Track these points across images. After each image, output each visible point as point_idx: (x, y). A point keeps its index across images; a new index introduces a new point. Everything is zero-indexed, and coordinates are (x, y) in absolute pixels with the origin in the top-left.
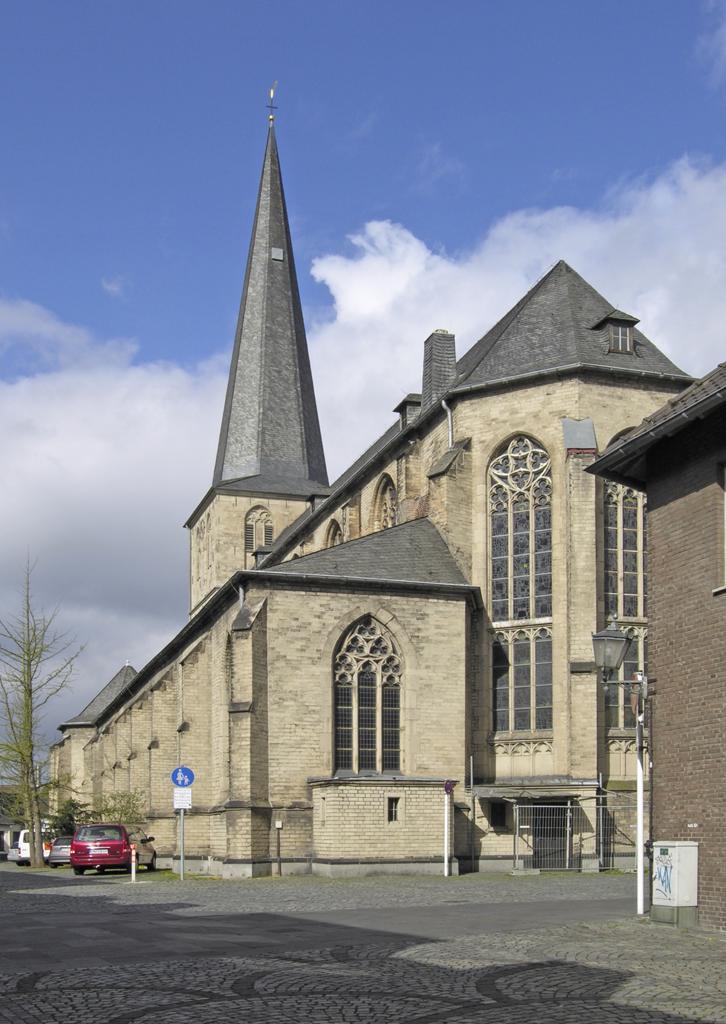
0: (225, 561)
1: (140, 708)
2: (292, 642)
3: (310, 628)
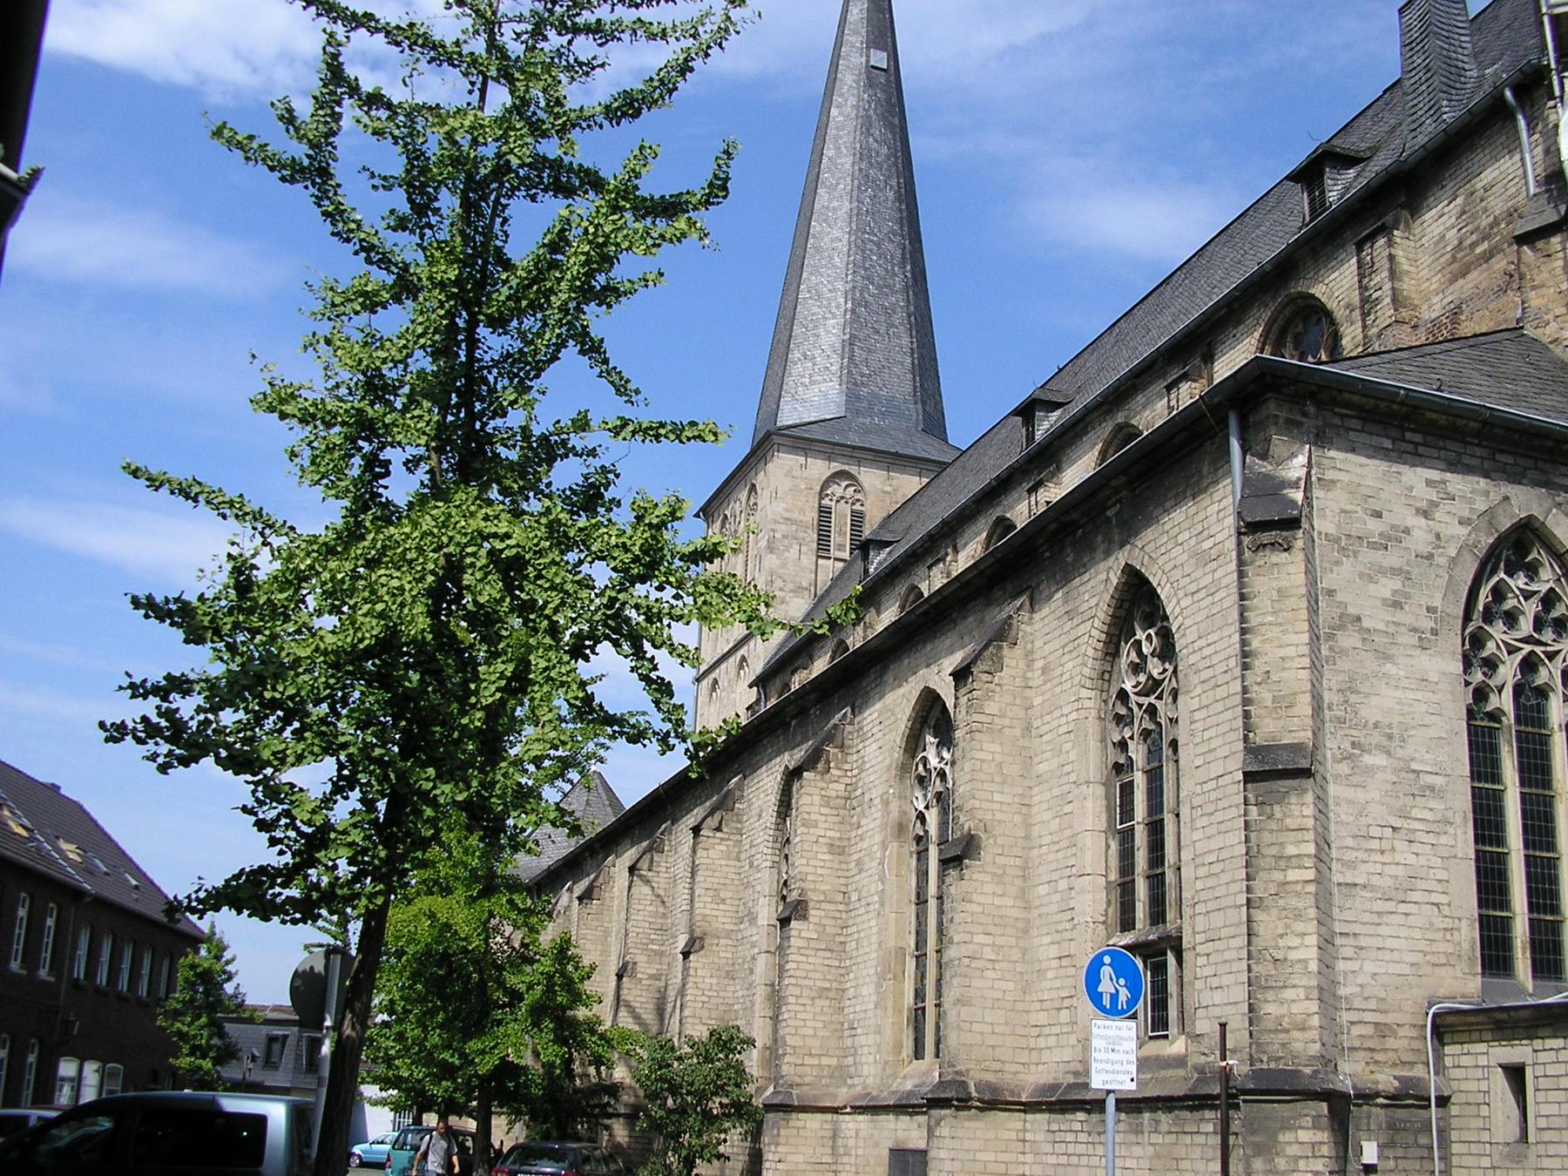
0: (781, 571)
1: (719, 829)
2: (1371, 579)
3: (1407, 542)
